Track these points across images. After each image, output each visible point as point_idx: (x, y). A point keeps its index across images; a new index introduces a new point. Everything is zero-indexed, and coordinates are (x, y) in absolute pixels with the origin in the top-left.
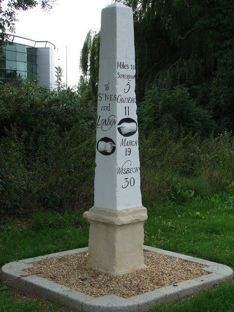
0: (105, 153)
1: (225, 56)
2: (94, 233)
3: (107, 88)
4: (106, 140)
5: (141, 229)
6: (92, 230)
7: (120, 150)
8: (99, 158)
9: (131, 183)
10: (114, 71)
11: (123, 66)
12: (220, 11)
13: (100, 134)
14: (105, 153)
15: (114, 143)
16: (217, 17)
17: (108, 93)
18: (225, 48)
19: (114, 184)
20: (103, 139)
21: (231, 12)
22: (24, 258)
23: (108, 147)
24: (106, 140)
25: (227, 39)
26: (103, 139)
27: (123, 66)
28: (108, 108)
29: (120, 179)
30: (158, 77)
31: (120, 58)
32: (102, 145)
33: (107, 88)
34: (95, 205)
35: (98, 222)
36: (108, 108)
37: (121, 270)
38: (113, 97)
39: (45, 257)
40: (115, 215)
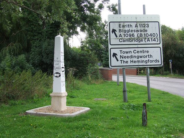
0: (57, 77)
1: (36, 43)
2: (53, 100)
3: (57, 59)
4: (57, 73)
5: (66, 98)
6: (53, 99)
7: (62, 76)
8: (55, 78)
9: (64, 85)
10: (60, 54)
11: (62, 53)
12: (33, 25)
13: (55, 71)
14: (57, 77)
15: (60, 74)
16: (31, 27)
17: (58, 60)
18: (35, 40)
19: (61, 85)
20: (56, 73)
21: (37, 25)
22: (33, 109)
23: (58, 75)
24: (57, 73)
25: (36, 36)
26: (56, 73)
27: (62, 53)
28: (58, 64)
29: (62, 83)
30: (3, 51)
31: (61, 51)
32: (56, 75)
33: (57, 59)
34: (53, 92)
35: (55, 96)
36: (58, 64)
37: (62, 110)
38: (59, 61)
39: (36, 109)
40: (61, 94)
